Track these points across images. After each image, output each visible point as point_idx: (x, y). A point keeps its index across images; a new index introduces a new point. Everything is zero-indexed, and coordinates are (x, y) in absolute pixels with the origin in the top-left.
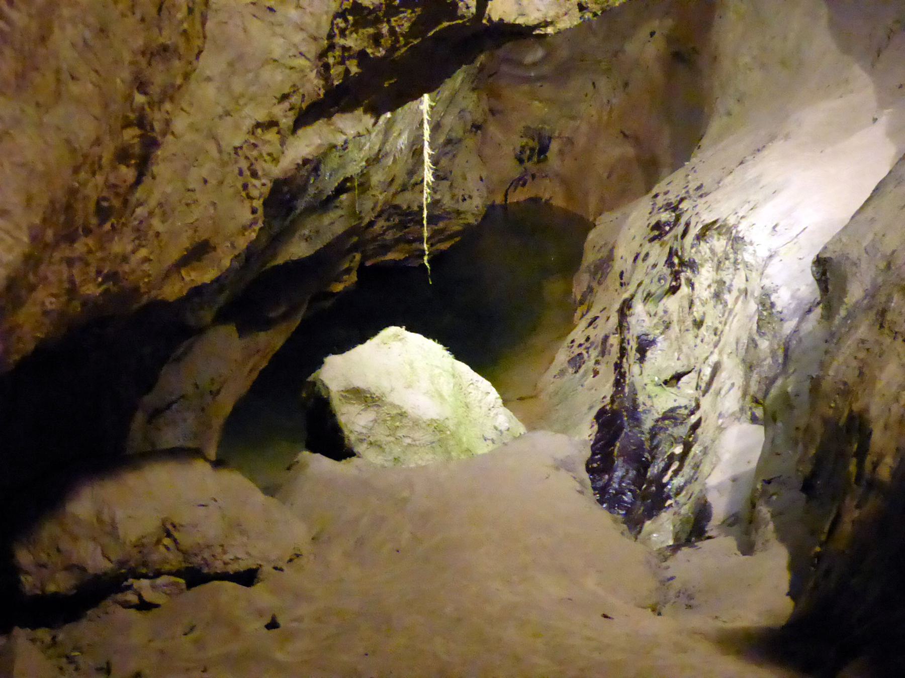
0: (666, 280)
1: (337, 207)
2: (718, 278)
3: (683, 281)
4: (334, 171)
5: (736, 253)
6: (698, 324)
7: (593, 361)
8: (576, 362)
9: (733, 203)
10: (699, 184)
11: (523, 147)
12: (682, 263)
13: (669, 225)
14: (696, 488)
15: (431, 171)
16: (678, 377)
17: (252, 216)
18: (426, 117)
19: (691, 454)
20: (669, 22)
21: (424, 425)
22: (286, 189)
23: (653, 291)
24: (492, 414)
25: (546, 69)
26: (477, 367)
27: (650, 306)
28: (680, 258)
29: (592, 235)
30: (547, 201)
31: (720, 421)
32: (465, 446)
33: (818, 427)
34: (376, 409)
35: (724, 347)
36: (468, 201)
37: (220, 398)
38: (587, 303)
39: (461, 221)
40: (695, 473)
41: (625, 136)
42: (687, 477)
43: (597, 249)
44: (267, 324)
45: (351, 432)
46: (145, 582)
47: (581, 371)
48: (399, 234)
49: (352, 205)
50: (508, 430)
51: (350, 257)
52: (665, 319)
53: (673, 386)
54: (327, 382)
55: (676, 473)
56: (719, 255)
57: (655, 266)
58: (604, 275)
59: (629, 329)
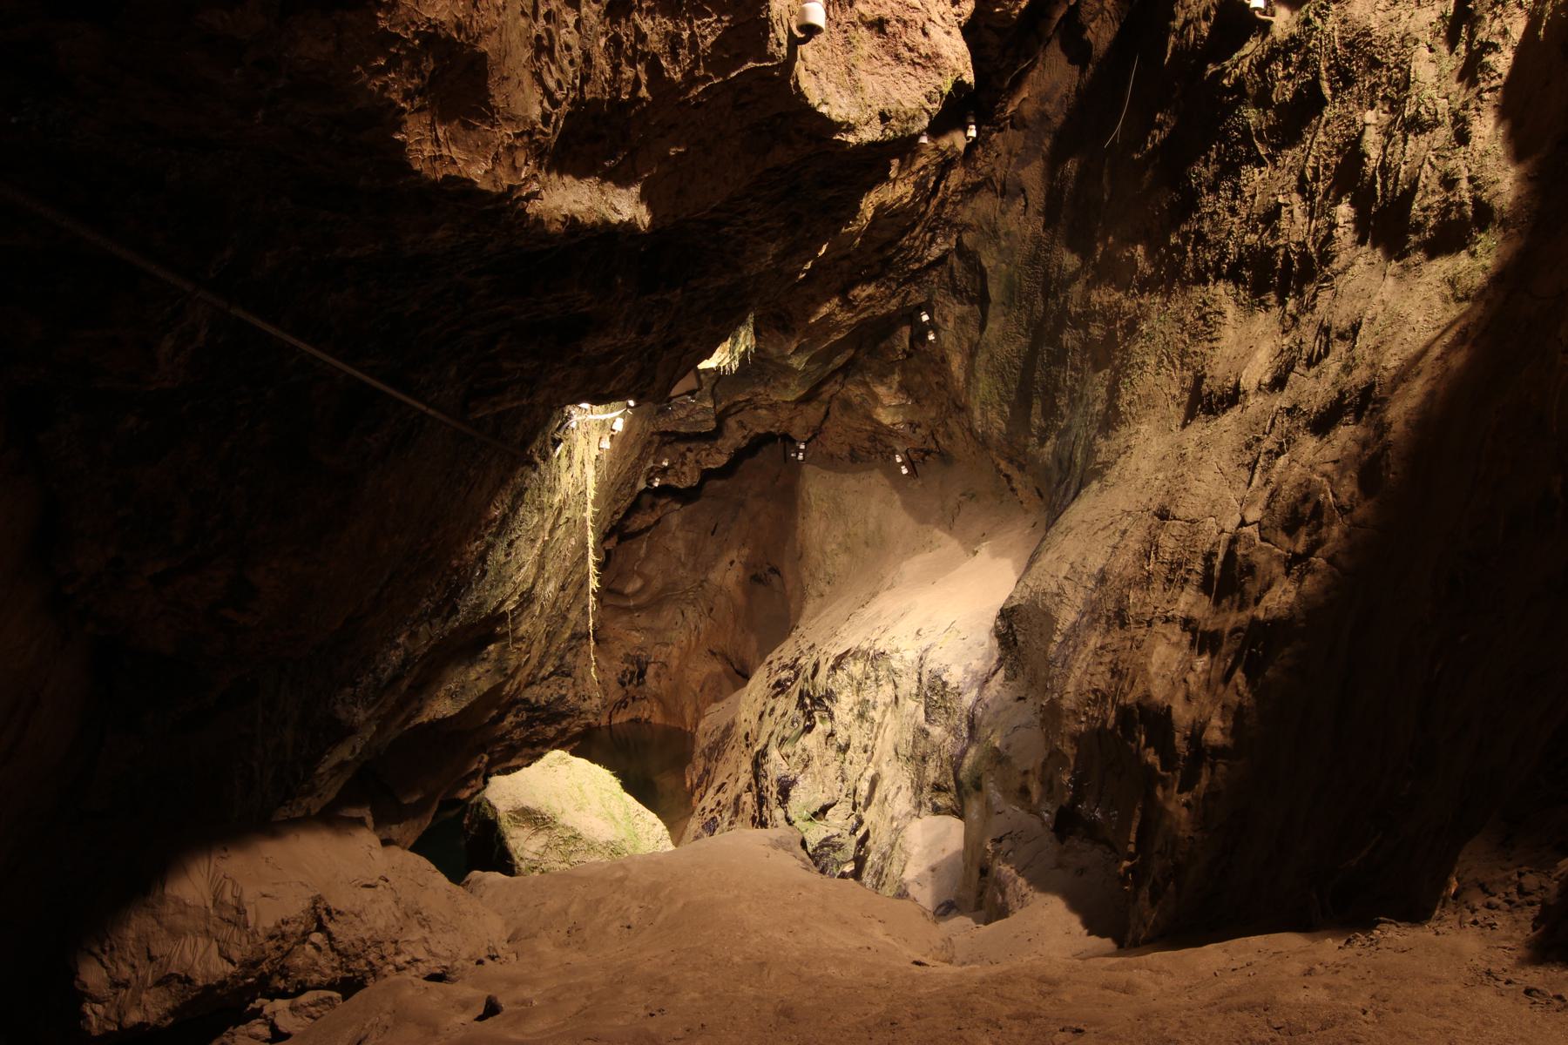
1: (484, 659)
6: (844, 749)
16: (824, 809)
18: (589, 523)
19: (868, 864)
20: (745, 552)
27: (787, 749)
28: (811, 698)
33: (1069, 750)
41: (713, 654)
46: (281, 1004)
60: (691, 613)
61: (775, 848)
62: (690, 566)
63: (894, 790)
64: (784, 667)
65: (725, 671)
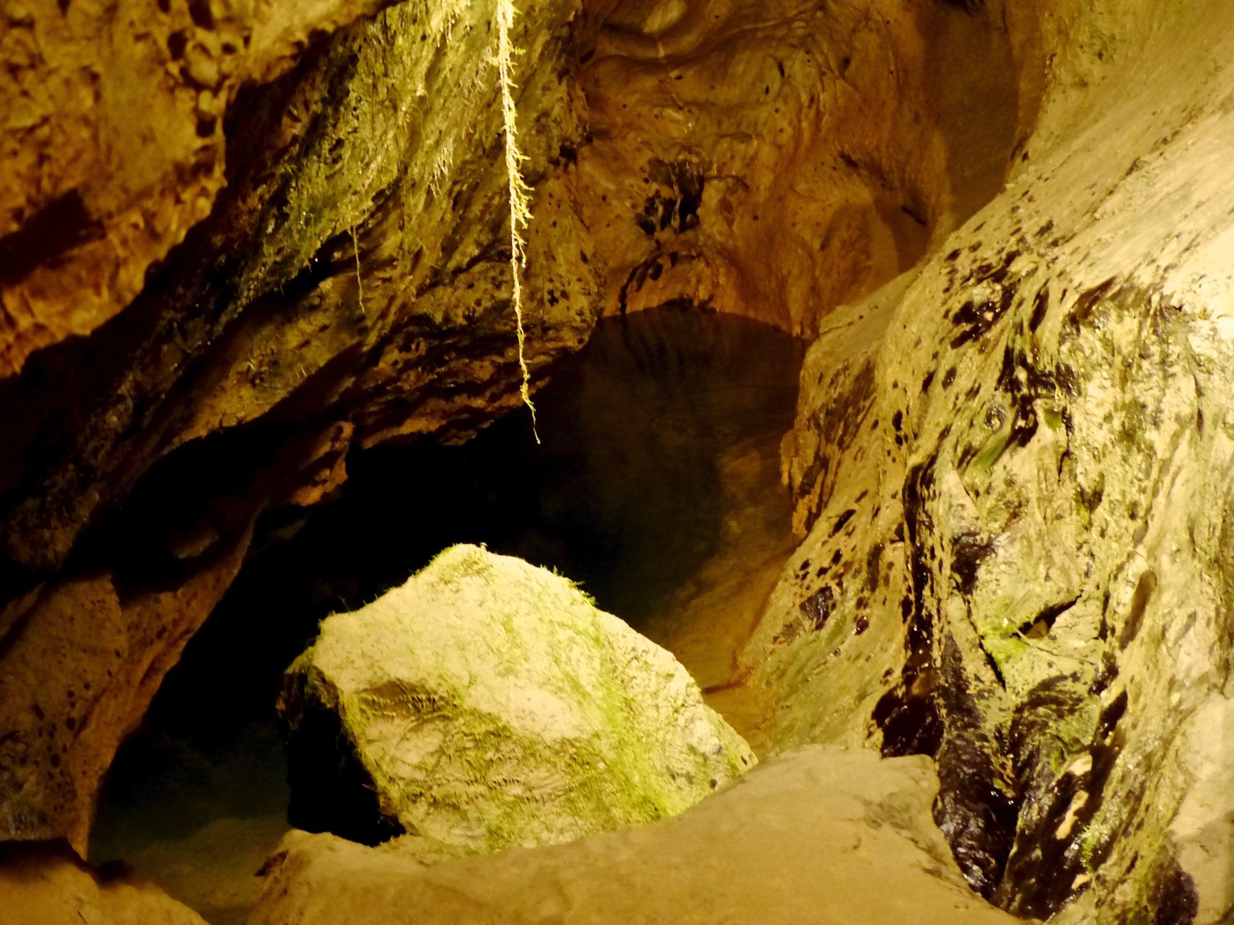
0: (1000, 416)
1: (313, 308)
2: (1128, 398)
4: (316, 212)
5: (1164, 341)
6: (1090, 500)
7: (853, 603)
8: (818, 607)
9: (1141, 244)
10: (1043, 223)
11: (651, 201)
12: (1037, 379)
13: (992, 309)
14: (1144, 844)
15: (525, 198)
16: (1049, 616)
17: (199, 143)
18: (506, 81)
19: (1116, 773)
21: (547, 753)
22: (218, 240)
23: (976, 444)
24: (681, 721)
25: (688, 41)
26: (637, 623)
27: (976, 475)
28: (1030, 370)
29: (813, 355)
30: (704, 305)
31: (1175, 697)
34: (440, 725)
35: (1161, 535)
36: (563, 303)
37: (86, 734)
38: (817, 488)
40: (1133, 812)
41: (851, 163)
42: (1114, 822)
43: (827, 380)
44: (174, 576)
45: (391, 780)
47: (831, 622)
48: (428, 378)
50: (719, 751)
51: (332, 431)
52: (1011, 496)
53: (1039, 636)
55: (1085, 816)
56: (1125, 351)
58: (852, 430)
59: (930, 527)
60: (799, 67)
61: (875, 824)
63: (1180, 618)
64: (984, 273)
65: (878, 202)
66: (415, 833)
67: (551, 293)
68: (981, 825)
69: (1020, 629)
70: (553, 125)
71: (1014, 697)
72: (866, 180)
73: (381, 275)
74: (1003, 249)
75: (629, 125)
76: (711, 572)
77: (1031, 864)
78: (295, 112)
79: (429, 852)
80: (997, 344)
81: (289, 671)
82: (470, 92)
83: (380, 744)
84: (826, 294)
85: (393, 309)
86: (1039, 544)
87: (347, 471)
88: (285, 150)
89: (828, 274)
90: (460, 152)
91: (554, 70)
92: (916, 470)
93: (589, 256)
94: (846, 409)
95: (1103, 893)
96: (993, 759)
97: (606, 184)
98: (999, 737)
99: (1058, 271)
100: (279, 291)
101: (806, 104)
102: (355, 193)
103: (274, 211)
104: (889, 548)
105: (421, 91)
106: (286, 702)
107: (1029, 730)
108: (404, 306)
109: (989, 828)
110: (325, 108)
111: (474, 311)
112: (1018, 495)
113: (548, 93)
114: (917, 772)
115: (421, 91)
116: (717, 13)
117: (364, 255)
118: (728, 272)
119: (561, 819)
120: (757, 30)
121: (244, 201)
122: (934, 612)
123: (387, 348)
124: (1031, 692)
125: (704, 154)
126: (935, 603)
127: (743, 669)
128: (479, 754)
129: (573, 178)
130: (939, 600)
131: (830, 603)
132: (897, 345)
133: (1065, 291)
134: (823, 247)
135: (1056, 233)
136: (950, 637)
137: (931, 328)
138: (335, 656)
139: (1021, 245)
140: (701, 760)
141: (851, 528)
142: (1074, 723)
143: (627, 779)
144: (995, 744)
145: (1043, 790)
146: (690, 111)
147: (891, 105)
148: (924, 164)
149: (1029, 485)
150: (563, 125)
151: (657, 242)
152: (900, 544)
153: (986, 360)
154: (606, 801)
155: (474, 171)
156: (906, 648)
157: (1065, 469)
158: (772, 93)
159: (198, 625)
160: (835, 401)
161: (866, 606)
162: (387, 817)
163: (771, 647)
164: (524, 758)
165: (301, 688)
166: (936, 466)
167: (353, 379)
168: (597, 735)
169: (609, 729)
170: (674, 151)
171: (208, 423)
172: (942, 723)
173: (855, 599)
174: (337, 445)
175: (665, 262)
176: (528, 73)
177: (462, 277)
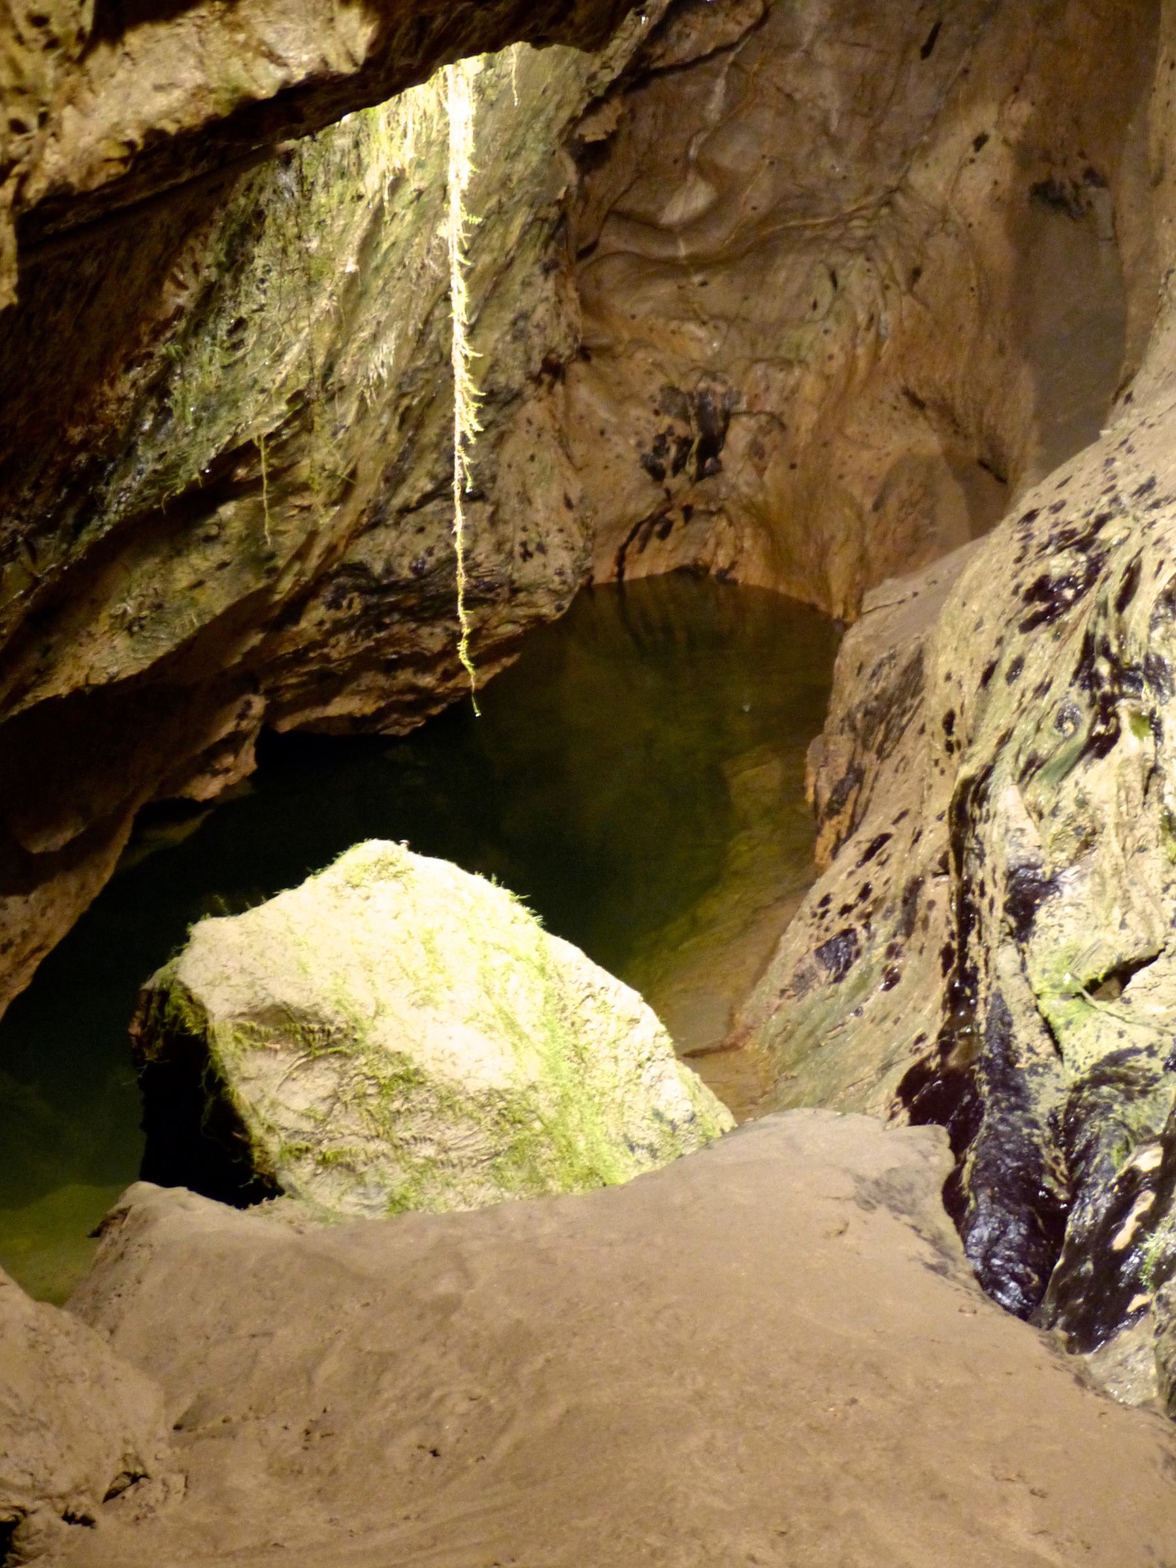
1: (209, 539)
3: (1125, 721)
4: (208, 412)
7: (882, 950)
8: (839, 953)
10: (1143, 479)
11: (661, 438)
12: (1122, 674)
13: (1072, 585)
16: (1123, 973)
20: (1022, 111)
21: (469, 1106)
23: (1043, 752)
24: (646, 1079)
27: (1040, 792)
28: (1114, 661)
29: (850, 641)
30: (722, 573)
32: (584, 1161)
36: (538, 559)
38: (849, 808)
39: (520, 612)
41: (917, 403)
43: (868, 671)
45: (270, 1129)
47: (853, 974)
48: (364, 644)
49: (253, 534)
50: (692, 1119)
51: (238, 707)
52: (1083, 820)
53: (1109, 997)
54: (199, 990)
55: (1150, 1222)
57: (1043, 689)
58: (895, 734)
59: (981, 856)
60: (857, 279)
62: (853, 147)
64: (1067, 540)
65: (948, 453)
66: (295, 1194)
67: (524, 544)
68: (1023, 1231)
69: (1086, 988)
70: (535, 331)
71: (1072, 1072)
72: (935, 425)
73: (298, 501)
74: (1091, 511)
75: (639, 343)
76: (712, 907)
77: (1079, 1280)
78: (181, 277)
79: (311, 1220)
80: (1075, 629)
81: (148, 985)
82: (419, 275)
83: (260, 1084)
84: (877, 566)
85: (317, 550)
86: (1115, 881)
87: (258, 758)
88: (167, 324)
89: (881, 542)
90: (406, 352)
91: (537, 260)
92: (966, 784)
93: (574, 501)
94: (889, 707)
95: (1165, 1318)
96: (1044, 1151)
97: (603, 414)
98: (1053, 1125)
99: (1154, 538)
100: (160, 509)
101: (864, 325)
102: (263, 391)
103: (153, 403)
104: (930, 882)
105: (351, 267)
106: (143, 1024)
107: (1088, 1114)
108: (331, 549)
109: (1034, 1232)
110: (221, 276)
111: (424, 563)
112: (1092, 819)
113: (530, 290)
114: (926, 1145)
115: (351, 267)
116: (754, 203)
117: (274, 476)
118: (755, 536)
119: (483, 1190)
120: (805, 227)
121: (112, 384)
122: (981, 964)
123: (312, 603)
124: (1094, 1068)
125: (731, 382)
126: (982, 952)
127: (739, 1030)
128: (384, 1103)
129: (561, 403)
130: (988, 949)
131: (854, 948)
132: (953, 628)
133: (1161, 563)
134: (876, 507)
135: (1159, 493)
136: (998, 996)
137: (997, 607)
138: (207, 968)
139: (1114, 506)
140: (668, 1129)
141: (884, 857)
142: (1146, 1108)
143: (570, 1144)
144: (1048, 1133)
145: (1100, 1188)
146: (716, 327)
147: (970, 331)
148: (1008, 405)
149: (1106, 807)
150: (548, 331)
151: (668, 491)
152: (944, 879)
153: (1061, 648)
154: (542, 1170)
155: (428, 381)
156: (944, 1008)
157: (1153, 789)
158: (822, 310)
159: (54, 941)
160: (877, 698)
161: (898, 955)
162: (262, 1175)
163: (777, 1002)
164: (440, 1111)
165: (161, 1008)
166: (992, 779)
167: (261, 636)
168: (533, 1087)
169: (550, 1080)
170: (694, 377)
171: (69, 678)
172: (982, 1104)
173: (886, 945)
174: (244, 724)
175: (676, 516)
176: (502, 260)
177: (411, 518)
